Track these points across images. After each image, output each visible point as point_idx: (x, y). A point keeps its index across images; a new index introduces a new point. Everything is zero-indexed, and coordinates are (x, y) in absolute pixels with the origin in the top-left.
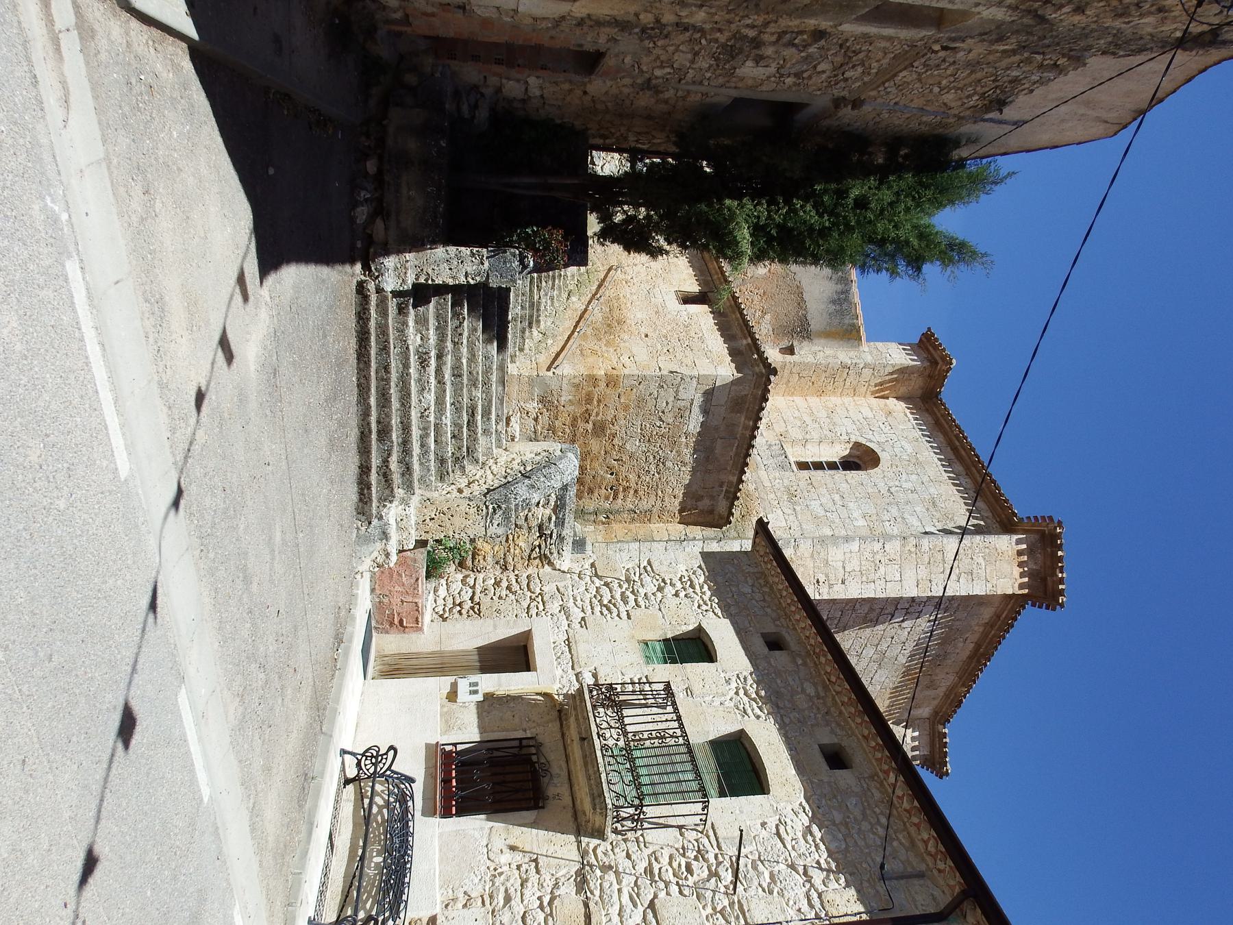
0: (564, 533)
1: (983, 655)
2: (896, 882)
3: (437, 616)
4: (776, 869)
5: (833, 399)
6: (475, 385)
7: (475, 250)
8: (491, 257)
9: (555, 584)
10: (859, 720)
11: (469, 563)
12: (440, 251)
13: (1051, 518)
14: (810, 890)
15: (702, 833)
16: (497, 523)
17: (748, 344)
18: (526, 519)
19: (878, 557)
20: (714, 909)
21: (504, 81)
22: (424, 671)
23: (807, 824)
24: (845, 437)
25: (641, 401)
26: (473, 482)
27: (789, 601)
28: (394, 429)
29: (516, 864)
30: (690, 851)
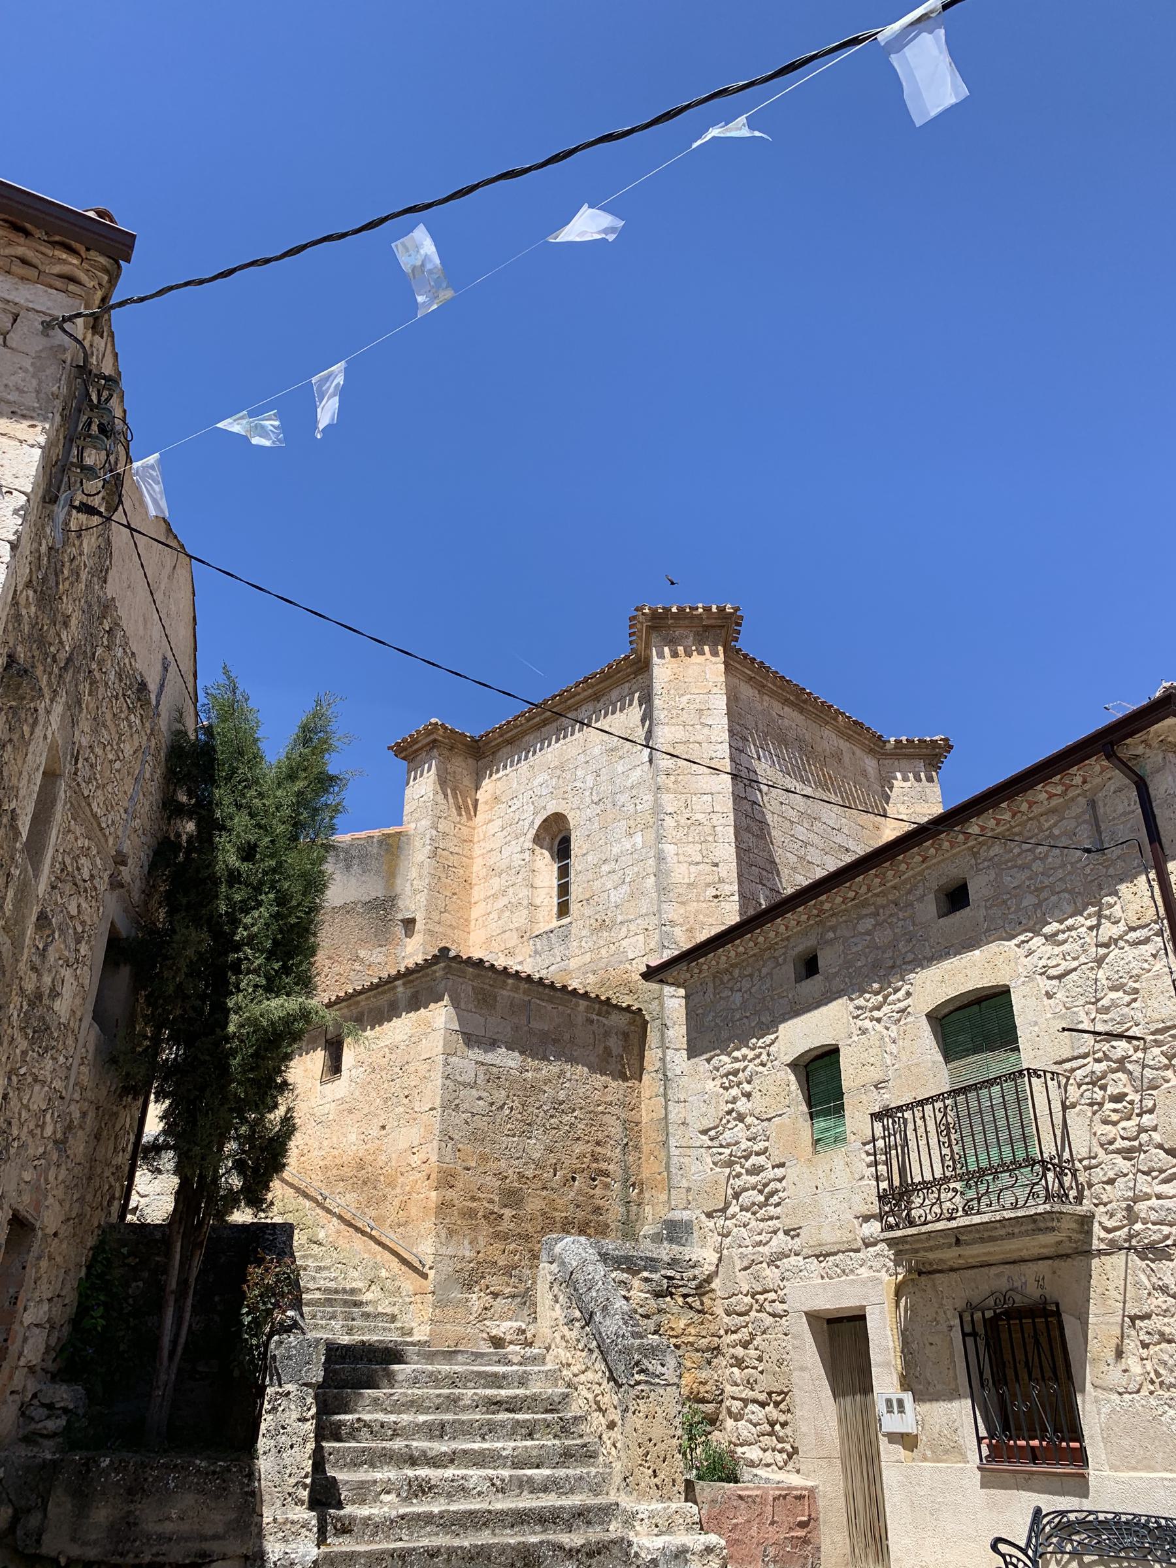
0: (666, 1258)
1: (797, 697)
2: (1104, 835)
3: (791, 1464)
4: (1105, 982)
5: (475, 869)
6: (456, 1400)
7: (266, 1406)
8: (279, 1380)
9: (738, 1274)
10: (903, 867)
11: (709, 1408)
12: (265, 1465)
13: (632, 619)
14: (1127, 941)
15: (1068, 1078)
16: (659, 1367)
17: (404, 984)
18: (647, 1317)
19: (683, 821)
20: (1167, 1067)
21: (22, 1362)
22: (873, 1488)
23: (1043, 940)
24: (527, 856)
25: (476, 1137)
26: (597, 1403)
27: (751, 944)
28: (522, 1539)
29: (1141, 1350)
30: (1095, 1096)
